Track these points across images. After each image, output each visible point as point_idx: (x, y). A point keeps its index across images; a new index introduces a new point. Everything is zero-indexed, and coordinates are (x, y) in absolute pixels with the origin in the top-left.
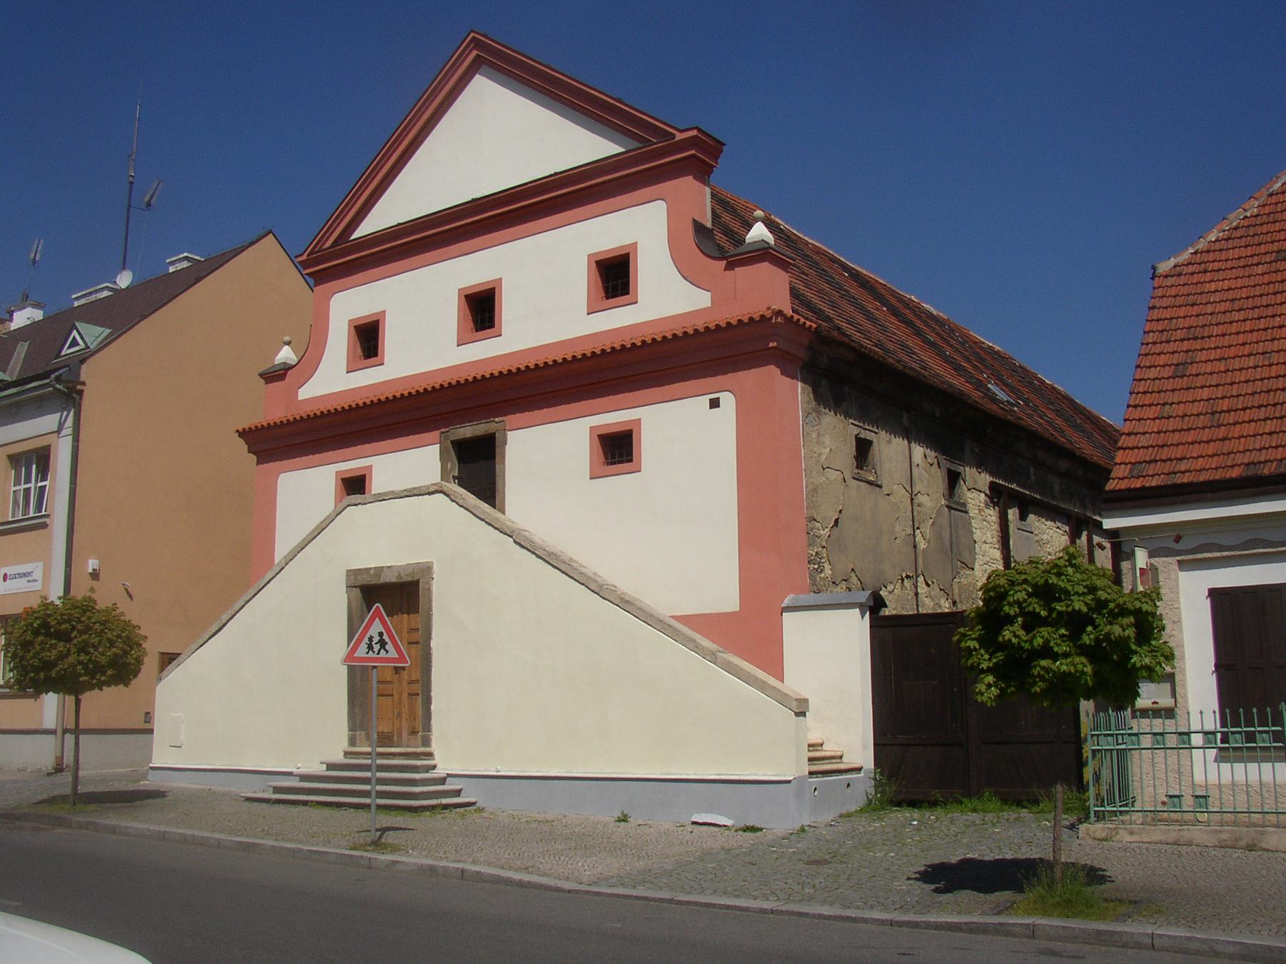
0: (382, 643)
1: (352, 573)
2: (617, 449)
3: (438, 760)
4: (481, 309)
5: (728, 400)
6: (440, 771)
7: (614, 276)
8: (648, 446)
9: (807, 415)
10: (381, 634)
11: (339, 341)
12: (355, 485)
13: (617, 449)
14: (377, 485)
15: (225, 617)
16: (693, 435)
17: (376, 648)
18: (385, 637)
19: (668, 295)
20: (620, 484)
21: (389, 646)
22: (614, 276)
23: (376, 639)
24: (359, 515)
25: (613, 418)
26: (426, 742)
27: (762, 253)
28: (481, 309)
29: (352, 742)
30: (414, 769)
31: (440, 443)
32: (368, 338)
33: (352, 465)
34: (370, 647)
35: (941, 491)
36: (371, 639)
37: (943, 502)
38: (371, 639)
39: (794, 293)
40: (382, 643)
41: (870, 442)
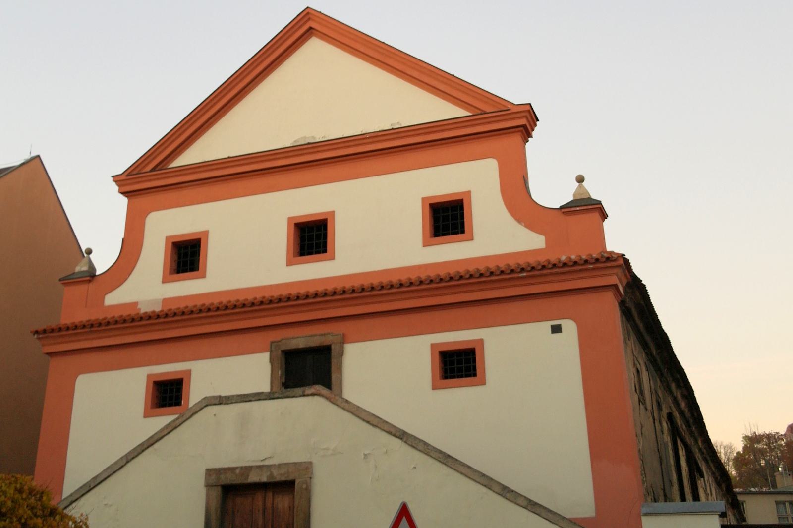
4: (312, 237)
5: (570, 327)
12: (168, 394)
14: (195, 394)
20: (461, 396)
28: (312, 237)
31: (271, 352)
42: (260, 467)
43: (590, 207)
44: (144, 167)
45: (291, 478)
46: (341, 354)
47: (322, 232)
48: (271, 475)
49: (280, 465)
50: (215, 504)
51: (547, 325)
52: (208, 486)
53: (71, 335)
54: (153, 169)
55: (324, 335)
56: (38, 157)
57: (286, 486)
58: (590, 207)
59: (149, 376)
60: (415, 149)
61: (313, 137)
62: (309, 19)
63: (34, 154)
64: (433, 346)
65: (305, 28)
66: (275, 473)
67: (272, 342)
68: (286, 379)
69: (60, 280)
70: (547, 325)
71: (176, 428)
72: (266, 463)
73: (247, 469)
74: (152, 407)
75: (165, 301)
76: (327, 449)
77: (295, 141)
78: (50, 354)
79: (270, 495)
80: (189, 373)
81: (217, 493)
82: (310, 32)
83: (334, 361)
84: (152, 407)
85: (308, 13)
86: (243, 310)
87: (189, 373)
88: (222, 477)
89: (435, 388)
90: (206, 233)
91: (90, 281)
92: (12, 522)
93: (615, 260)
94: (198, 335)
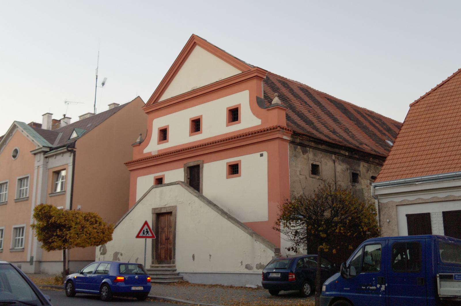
0: (147, 232)
1: (154, 209)
2: (234, 169)
3: (177, 268)
4: (196, 125)
5: (265, 154)
6: (177, 272)
7: (234, 115)
8: (243, 169)
9: (290, 157)
10: (147, 229)
11: (155, 135)
12: (159, 181)
13: (234, 169)
14: (166, 181)
15: (117, 224)
16: (256, 165)
17: (146, 233)
18: (148, 230)
19: (249, 121)
20: (235, 180)
21: (149, 233)
22: (234, 115)
23: (146, 231)
24: (159, 190)
25: (233, 160)
26: (174, 263)
27: (277, 107)
28: (196, 125)
29: (153, 263)
30: (19, 243)
31: (184, 167)
32: (164, 134)
33: (159, 175)
34: (144, 233)
35: (349, 180)
36: (144, 231)
37: (350, 184)
38: (144, 231)
39: (288, 117)
40: (147, 232)
41: (318, 166)
42: (164, 207)
43: (274, 107)
44: (150, 103)
45: (171, 211)
46: (203, 167)
47: (236, 113)
48: (167, 210)
49: (169, 207)
50: (154, 219)
51: (259, 154)
52: (153, 214)
53: (260, 135)
54: (154, 103)
55: (198, 161)
56: (139, 96)
57: (170, 213)
58: (274, 107)
59: (227, 163)
60: (225, 88)
61: (197, 87)
62: (194, 39)
63: (138, 96)
64: (227, 163)
65: (194, 42)
66: (168, 209)
67: (184, 164)
68: (190, 176)
69: (132, 145)
70: (259, 154)
71: (146, 195)
72: (166, 206)
73: (161, 208)
74: (229, 175)
75: (159, 151)
76: (180, 202)
77: (192, 89)
78: (131, 171)
79: (169, 216)
80: (164, 175)
81: (155, 215)
82: (195, 44)
83: (200, 170)
84: (229, 175)
85: (193, 36)
86: (252, 135)
87: (164, 175)
88: (156, 211)
89: (227, 178)
90: (168, 126)
91: (139, 145)
92: (78, 226)
93: (277, 128)
94: (217, 151)
